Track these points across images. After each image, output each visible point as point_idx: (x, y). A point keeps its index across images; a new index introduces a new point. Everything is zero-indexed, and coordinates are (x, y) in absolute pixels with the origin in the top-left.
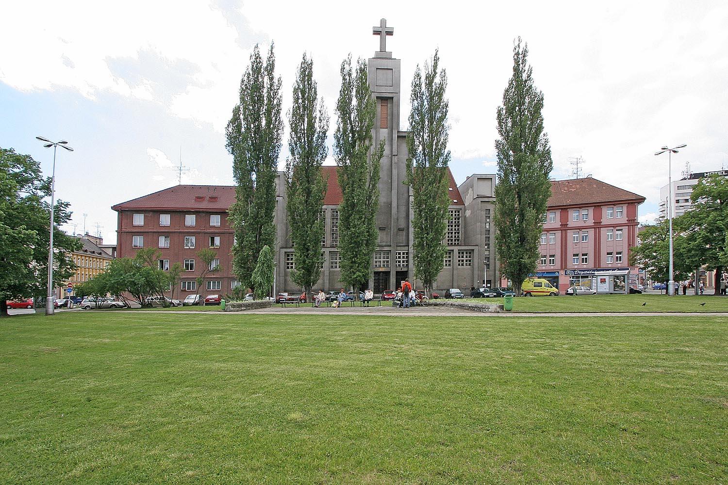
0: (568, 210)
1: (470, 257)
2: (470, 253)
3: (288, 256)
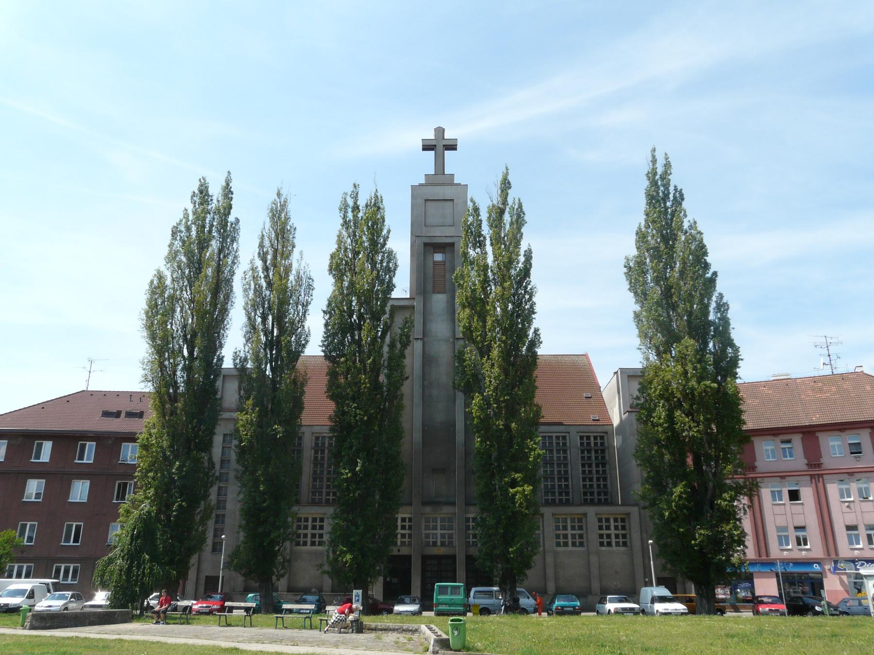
2: (623, 520)
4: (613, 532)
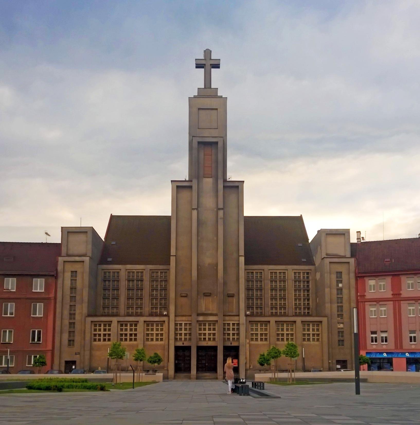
0: (365, 278)
1: (318, 330)
2: (318, 325)
3: (95, 325)
4: (311, 332)
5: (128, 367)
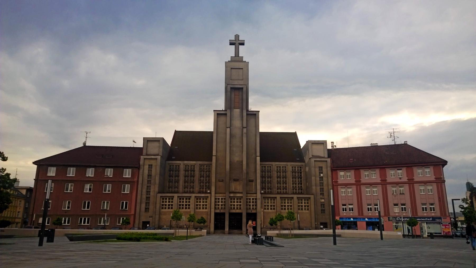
5: (184, 226)
